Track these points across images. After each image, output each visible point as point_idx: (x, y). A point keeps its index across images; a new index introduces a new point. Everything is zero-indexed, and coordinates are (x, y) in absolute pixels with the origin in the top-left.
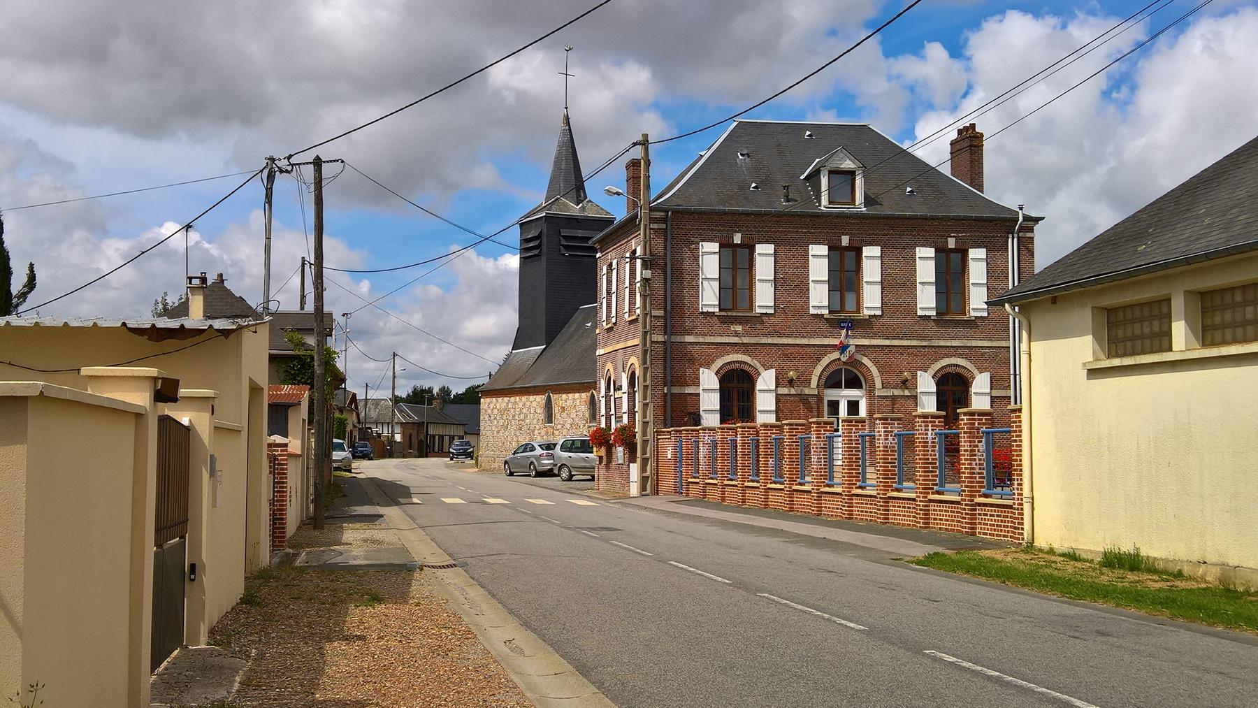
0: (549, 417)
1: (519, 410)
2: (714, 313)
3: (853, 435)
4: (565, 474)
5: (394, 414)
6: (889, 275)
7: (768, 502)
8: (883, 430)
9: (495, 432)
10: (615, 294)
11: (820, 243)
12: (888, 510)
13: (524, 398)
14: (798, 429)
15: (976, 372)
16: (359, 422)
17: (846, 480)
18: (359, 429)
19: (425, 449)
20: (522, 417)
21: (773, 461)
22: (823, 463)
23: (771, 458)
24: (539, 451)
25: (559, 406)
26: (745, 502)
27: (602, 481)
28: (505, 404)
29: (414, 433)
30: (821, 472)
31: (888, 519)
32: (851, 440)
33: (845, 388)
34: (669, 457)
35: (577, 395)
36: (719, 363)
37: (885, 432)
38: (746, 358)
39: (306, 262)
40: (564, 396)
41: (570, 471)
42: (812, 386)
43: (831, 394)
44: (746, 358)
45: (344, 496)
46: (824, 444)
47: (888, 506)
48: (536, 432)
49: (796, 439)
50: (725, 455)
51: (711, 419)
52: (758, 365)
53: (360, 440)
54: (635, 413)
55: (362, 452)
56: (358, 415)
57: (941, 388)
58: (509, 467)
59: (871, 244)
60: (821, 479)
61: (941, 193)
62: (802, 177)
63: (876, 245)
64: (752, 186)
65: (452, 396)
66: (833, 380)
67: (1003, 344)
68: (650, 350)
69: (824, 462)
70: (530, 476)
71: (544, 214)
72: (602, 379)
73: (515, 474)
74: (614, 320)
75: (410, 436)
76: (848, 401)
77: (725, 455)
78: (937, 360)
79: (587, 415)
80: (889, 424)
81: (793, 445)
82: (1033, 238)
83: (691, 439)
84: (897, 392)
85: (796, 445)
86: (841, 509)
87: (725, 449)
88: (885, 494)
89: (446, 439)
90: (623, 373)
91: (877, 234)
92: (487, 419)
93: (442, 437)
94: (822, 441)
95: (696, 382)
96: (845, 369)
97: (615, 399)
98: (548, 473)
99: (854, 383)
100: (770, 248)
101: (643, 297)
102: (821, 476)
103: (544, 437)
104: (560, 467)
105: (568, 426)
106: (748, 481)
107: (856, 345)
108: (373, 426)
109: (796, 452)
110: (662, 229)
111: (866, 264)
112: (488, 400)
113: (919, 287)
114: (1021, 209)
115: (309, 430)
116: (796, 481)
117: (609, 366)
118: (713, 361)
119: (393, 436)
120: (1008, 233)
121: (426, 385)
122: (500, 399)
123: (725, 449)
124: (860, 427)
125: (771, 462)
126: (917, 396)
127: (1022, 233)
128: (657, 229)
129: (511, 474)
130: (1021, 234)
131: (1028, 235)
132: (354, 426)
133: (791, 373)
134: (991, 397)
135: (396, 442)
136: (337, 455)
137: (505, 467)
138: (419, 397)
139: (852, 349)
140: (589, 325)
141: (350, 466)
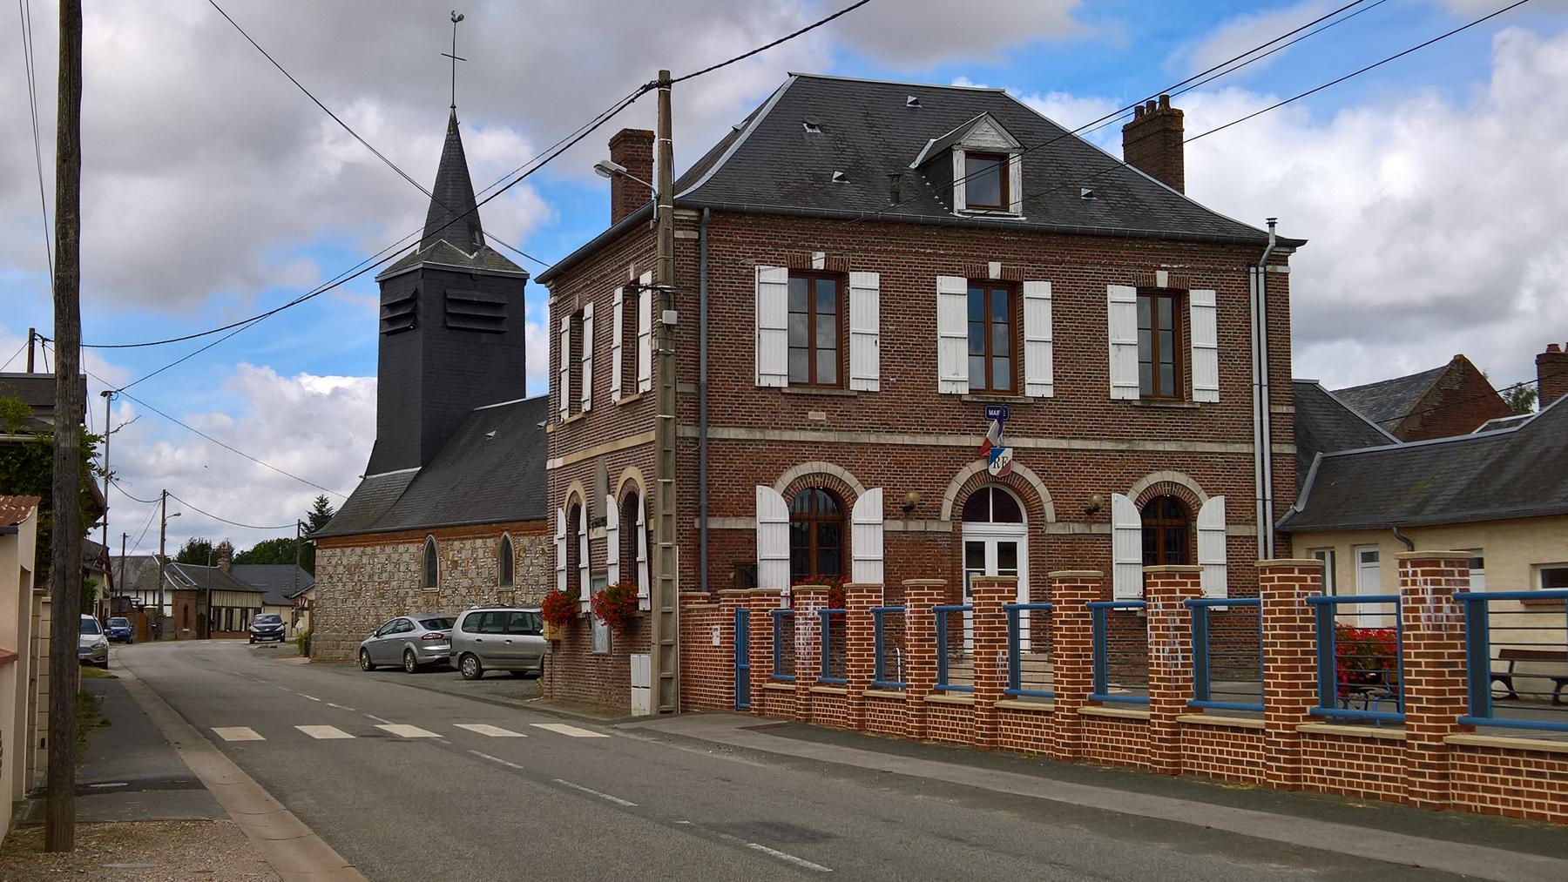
0: (431, 577)
1: (379, 566)
2: (780, 389)
3: (1296, 599)
4: (470, 668)
5: (162, 577)
6: (1065, 329)
7: (995, 736)
8: (1430, 587)
9: (339, 602)
10: (590, 361)
11: (953, 274)
12: (1445, 776)
13: (388, 549)
14: (1087, 588)
15: (1202, 495)
16: (112, 589)
17: (982, 684)
18: (112, 599)
19: (206, 627)
20: (385, 576)
21: (1004, 653)
22: (1180, 661)
23: (1000, 647)
24: (421, 631)
25: (447, 560)
26: (925, 734)
27: (559, 681)
28: (356, 558)
29: (192, 604)
30: (1177, 680)
31: (1446, 796)
32: (1293, 612)
33: (994, 521)
34: (716, 642)
35: (479, 542)
36: (789, 476)
37: (1435, 591)
38: (833, 469)
39: (36, 337)
40: (457, 544)
41: (479, 664)
42: (943, 518)
43: (973, 531)
44: (833, 469)
45: (105, 723)
46: (1182, 621)
47: (1445, 767)
48: (409, 601)
49: (1083, 609)
50: (864, 639)
51: (775, 574)
52: (849, 478)
53: (113, 614)
54: (578, 571)
55: (117, 631)
56: (110, 578)
57: (1147, 521)
58: (368, 656)
59: (1035, 278)
60: (1177, 695)
61: (1136, 199)
62: (913, 166)
63: (1045, 279)
64: (834, 177)
65: (234, 556)
66: (974, 508)
67: (1245, 448)
68: (674, 451)
69: (1184, 658)
70: (402, 669)
71: (421, 266)
72: (560, 509)
73: (377, 668)
74: (587, 407)
75: (186, 608)
76: (998, 543)
77: (864, 639)
78: (1141, 475)
79: (496, 572)
80: (1442, 573)
81: (1077, 623)
82: (1287, 274)
83: (767, 610)
84: (1078, 528)
85: (1083, 622)
86: (794, 703)
87: (864, 629)
88: (1439, 739)
89: (237, 612)
90: (609, 497)
91: (1045, 261)
92: (325, 581)
93: (230, 610)
94: (1179, 614)
95: (749, 509)
96: (993, 488)
97: (589, 541)
98: (439, 666)
99: (1007, 513)
100: (871, 280)
101: (660, 358)
102: (1178, 688)
103: (422, 609)
104: (462, 656)
105: (464, 592)
106: (931, 693)
107: (1015, 448)
108: (133, 595)
109: (1083, 636)
110: (692, 240)
111: (1029, 308)
112: (329, 552)
113: (1112, 350)
114: (1272, 224)
115: (36, 594)
116: (1452, 720)
117: (576, 486)
118: (779, 474)
119: (161, 609)
120: (1250, 266)
121: (206, 539)
122: (348, 551)
123: (864, 629)
124: (1309, 582)
125: (1001, 655)
126: (1111, 535)
127: (1271, 267)
128: (683, 239)
129: (372, 668)
130: (1269, 268)
131: (1280, 269)
132: (106, 596)
133: (911, 495)
134: (1227, 537)
135: (165, 617)
136: (87, 639)
137: (361, 656)
138: (197, 554)
139: (1008, 454)
140: (492, 434)
141: (105, 656)
